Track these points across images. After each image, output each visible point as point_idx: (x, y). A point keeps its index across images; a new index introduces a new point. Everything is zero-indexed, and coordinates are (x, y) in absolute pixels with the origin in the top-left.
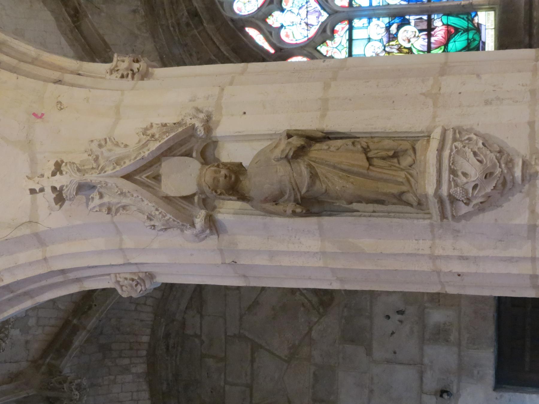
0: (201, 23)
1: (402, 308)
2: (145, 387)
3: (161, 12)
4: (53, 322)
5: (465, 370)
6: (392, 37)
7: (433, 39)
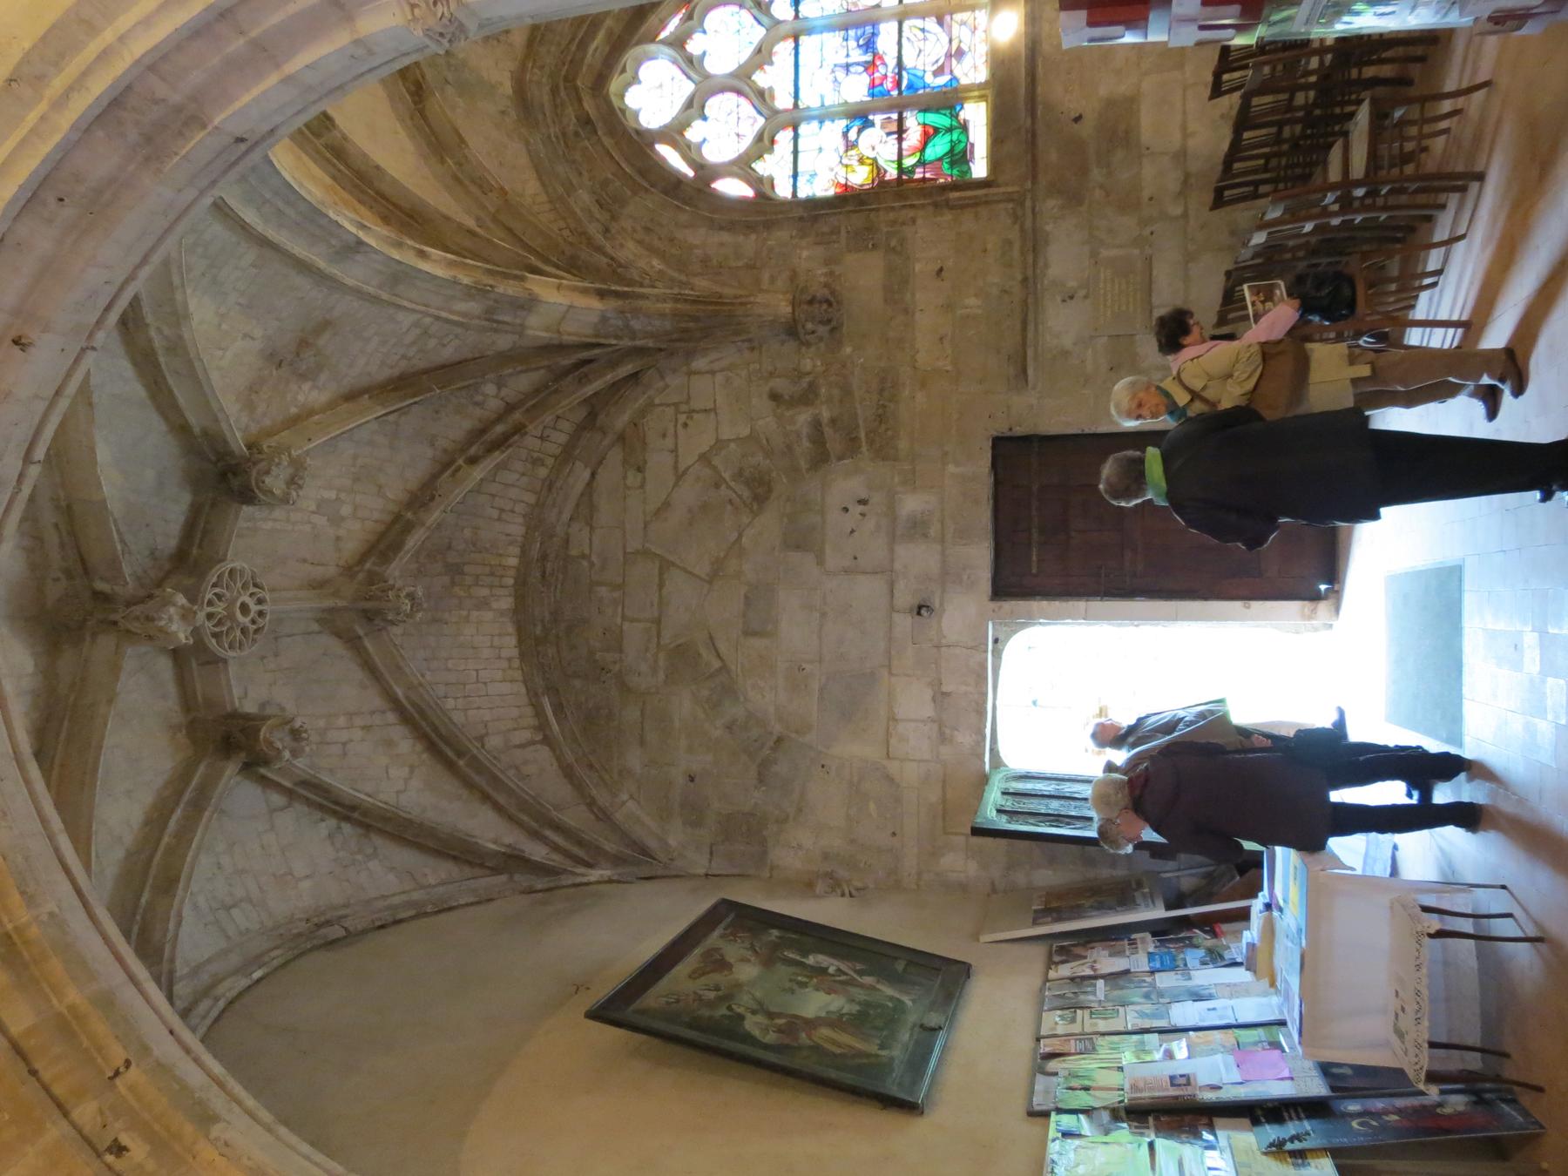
0: (596, 132)
1: (863, 496)
2: (511, 629)
3: (540, 117)
4: (376, 516)
5: (949, 575)
6: (850, 146)
7: (905, 145)
